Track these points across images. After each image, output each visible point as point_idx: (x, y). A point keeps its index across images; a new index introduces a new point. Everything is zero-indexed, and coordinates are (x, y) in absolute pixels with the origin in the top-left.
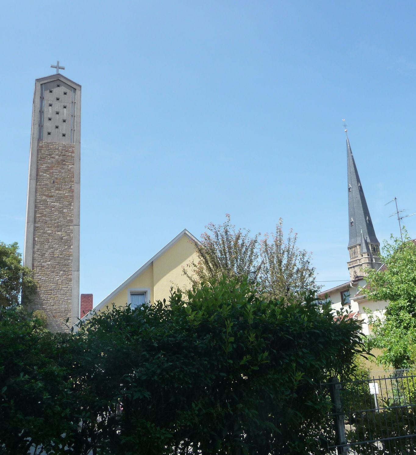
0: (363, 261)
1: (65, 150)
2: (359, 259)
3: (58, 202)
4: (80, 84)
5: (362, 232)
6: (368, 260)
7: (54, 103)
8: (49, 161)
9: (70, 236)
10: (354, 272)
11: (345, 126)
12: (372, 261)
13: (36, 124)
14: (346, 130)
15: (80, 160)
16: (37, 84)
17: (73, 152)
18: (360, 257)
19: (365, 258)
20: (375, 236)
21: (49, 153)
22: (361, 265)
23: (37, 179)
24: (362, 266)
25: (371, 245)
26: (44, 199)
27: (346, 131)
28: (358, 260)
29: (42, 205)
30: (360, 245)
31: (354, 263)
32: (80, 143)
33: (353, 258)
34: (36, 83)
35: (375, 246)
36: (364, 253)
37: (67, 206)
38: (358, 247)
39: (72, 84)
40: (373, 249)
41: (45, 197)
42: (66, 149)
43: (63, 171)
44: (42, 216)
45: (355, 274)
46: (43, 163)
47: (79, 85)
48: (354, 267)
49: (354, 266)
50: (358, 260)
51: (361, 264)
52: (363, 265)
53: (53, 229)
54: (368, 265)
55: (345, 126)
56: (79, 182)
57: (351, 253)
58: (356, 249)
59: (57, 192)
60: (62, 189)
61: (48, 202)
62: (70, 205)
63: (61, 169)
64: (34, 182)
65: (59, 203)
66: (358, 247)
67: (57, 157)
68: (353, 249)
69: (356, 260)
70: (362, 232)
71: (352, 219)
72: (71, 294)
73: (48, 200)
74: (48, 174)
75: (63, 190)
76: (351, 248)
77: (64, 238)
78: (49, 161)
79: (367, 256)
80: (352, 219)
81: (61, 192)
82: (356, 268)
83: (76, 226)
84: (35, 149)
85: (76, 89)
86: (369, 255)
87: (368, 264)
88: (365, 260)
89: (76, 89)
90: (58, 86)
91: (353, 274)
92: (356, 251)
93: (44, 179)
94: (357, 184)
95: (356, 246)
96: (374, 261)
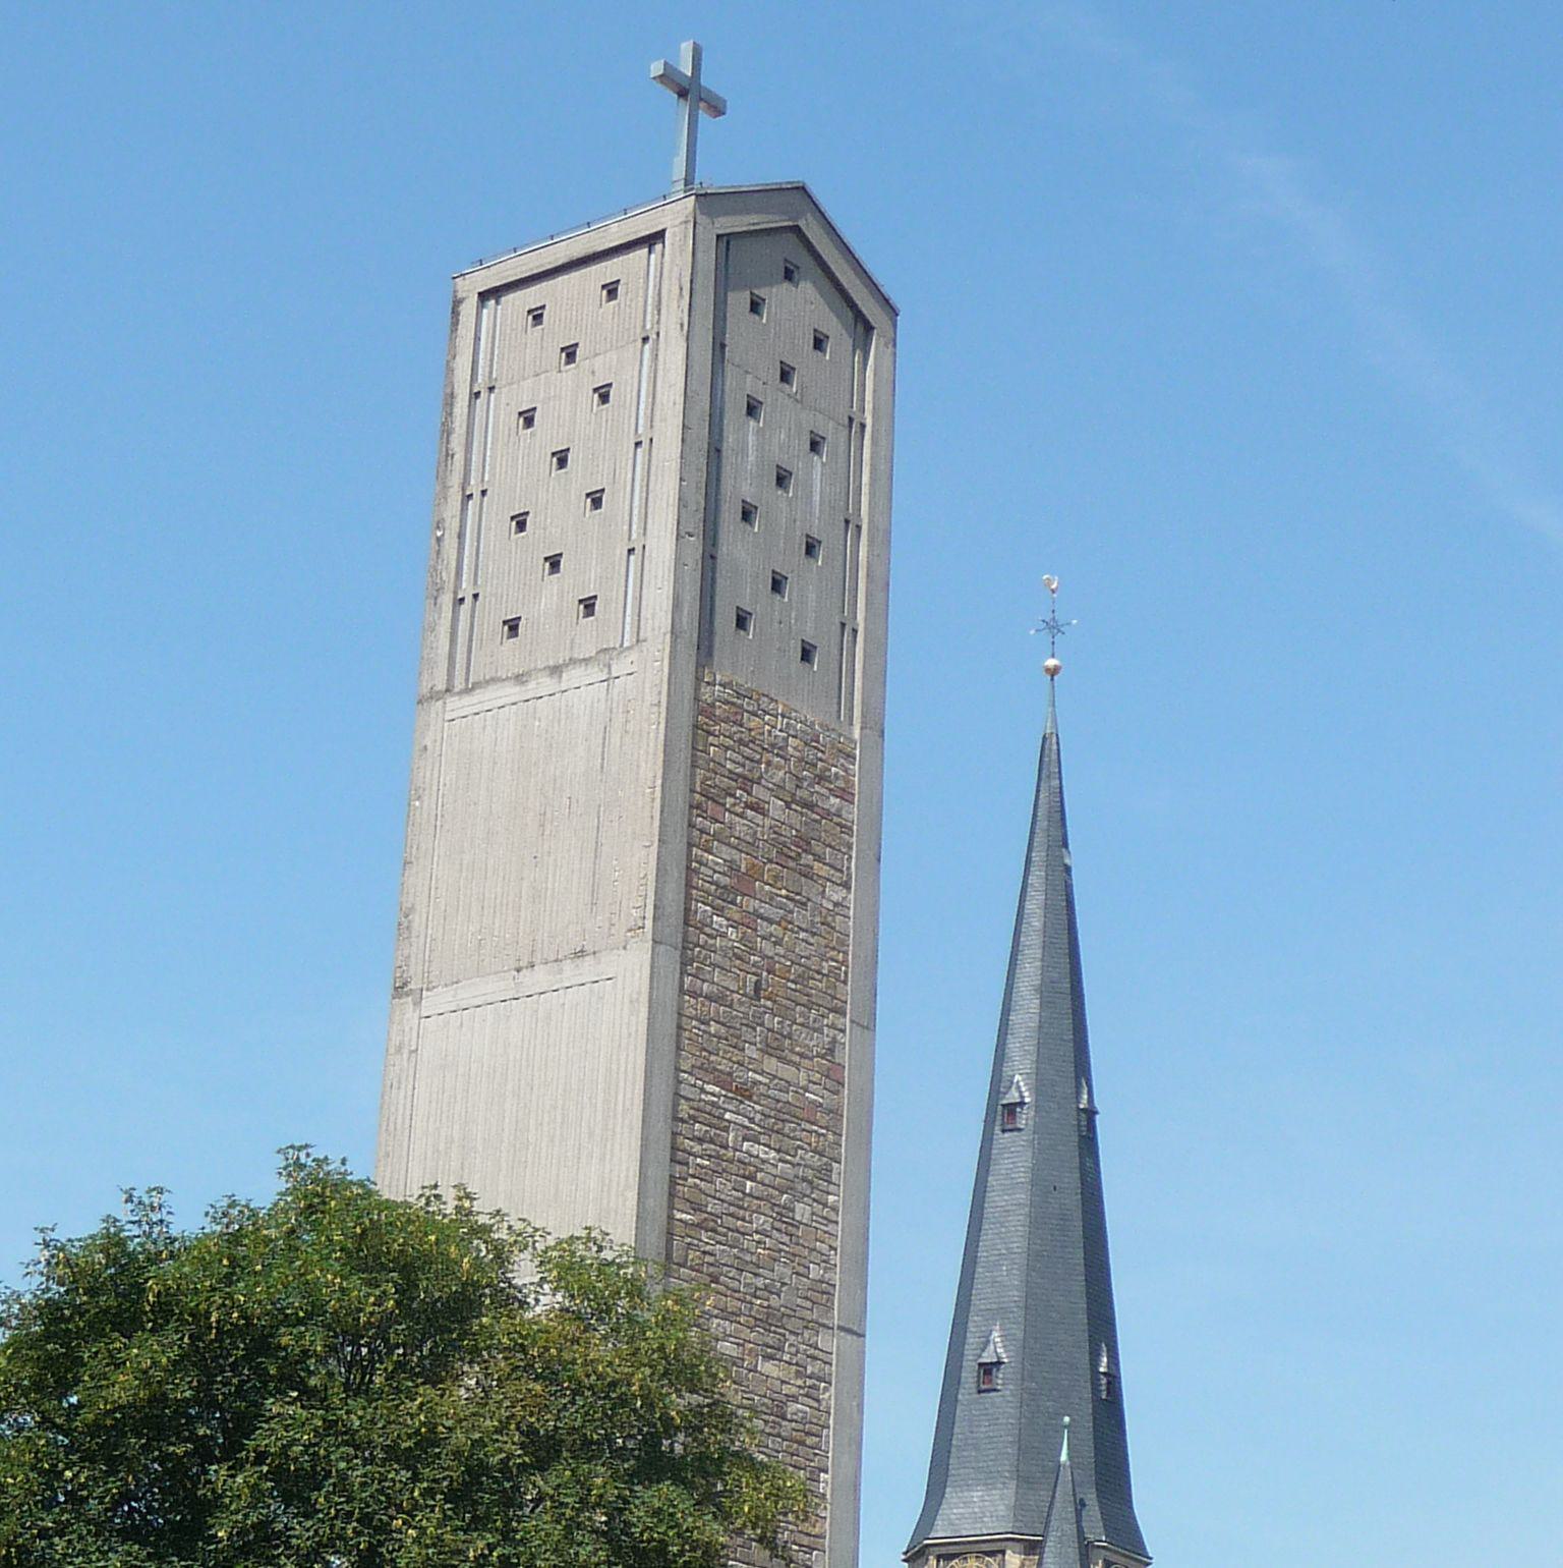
1: (815, 765)
3: (774, 1140)
4: (896, 299)
5: (1064, 1457)
8: (741, 827)
9: (818, 1401)
11: (1053, 627)
14: (1051, 662)
15: (879, 860)
16: (700, 229)
17: (845, 794)
20: (1131, 1507)
21: (739, 770)
23: (686, 945)
26: (713, 1104)
27: (1053, 672)
29: (700, 1140)
32: (882, 734)
37: (810, 1183)
39: (851, 274)
41: (718, 1089)
42: (820, 764)
43: (799, 917)
46: (716, 837)
47: (887, 301)
53: (746, 1333)
55: (1053, 627)
56: (867, 1024)
59: (770, 1065)
60: (792, 1051)
61: (726, 1130)
62: (825, 1173)
63: (791, 905)
64: (671, 960)
65: (778, 1151)
67: (776, 806)
70: (1064, 1457)
71: (996, 1336)
73: (727, 1116)
74: (734, 925)
75: (797, 1059)
76: (950, 1557)
77: (793, 1407)
80: (996, 1336)
81: (787, 1072)
83: (849, 1337)
84: (685, 719)
85: (872, 328)
89: (872, 328)
90: (789, 275)
94: (1071, 1090)
95: (1003, 1552)
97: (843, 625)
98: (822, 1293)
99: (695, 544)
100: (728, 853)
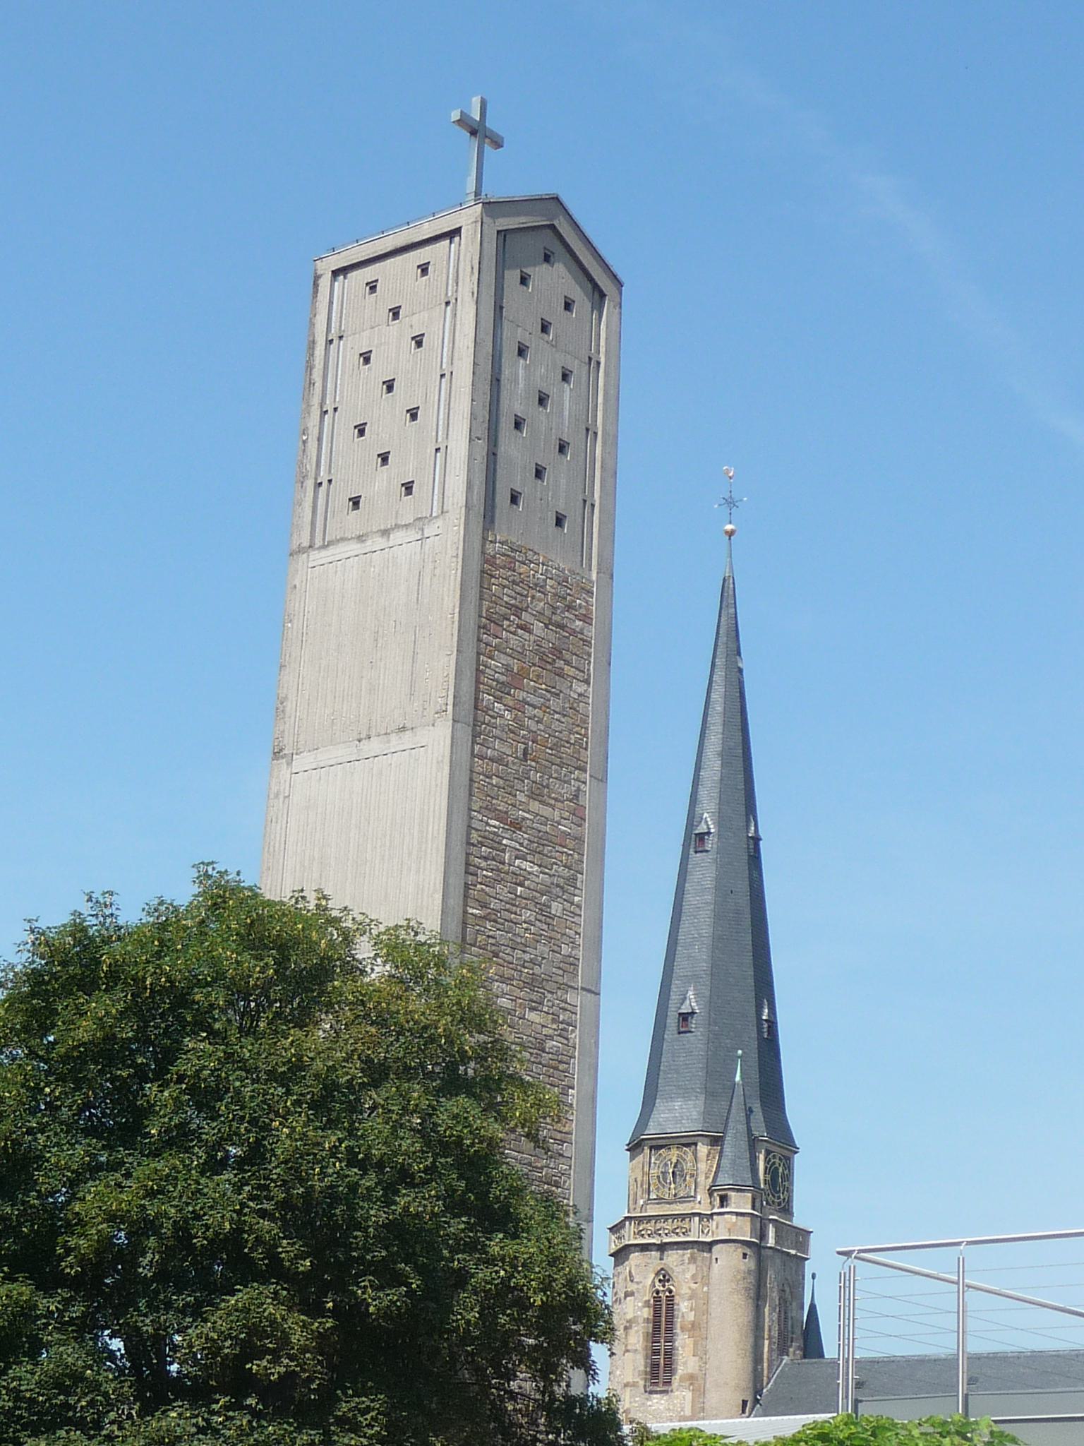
0: (720, 1229)
1: (565, 599)
2: (699, 1214)
3: (537, 858)
5: (738, 1078)
6: (748, 1228)
7: (533, 345)
8: (514, 641)
9: (567, 1039)
10: (657, 1274)
11: (730, 503)
12: (763, 1236)
13: (479, 435)
14: (729, 527)
15: (610, 664)
17: (586, 619)
18: (702, 1204)
19: (737, 1214)
22: (709, 1246)
23: (476, 723)
24: (710, 1251)
25: (768, 1152)
26: (495, 833)
27: (730, 534)
28: (697, 1219)
29: (486, 859)
30: (716, 1141)
31: (669, 1225)
32: (612, 576)
33: (660, 1200)
34: (485, 218)
35: (777, 1161)
36: (738, 1190)
37: (562, 888)
38: (703, 1149)
40: (768, 1178)
42: (569, 598)
43: (554, 703)
44: (485, 918)
45: (659, 1286)
46: (496, 648)
47: (615, 276)
48: (662, 1248)
49: (666, 1244)
50: (697, 1219)
51: (708, 1239)
52: (716, 1248)
53: (517, 992)
54: (745, 1256)
55: (730, 503)
56: (601, 778)
57: (654, 1171)
58: (690, 1156)
59: (534, 806)
61: (504, 851)
63: (548, 695)
64: (465, 733)
65: (540, 866)
66: (703, 1149)
67: (538, 627)
68: (674, 1154)
69: (683, 1217)
70: (738, 1078)
71: (691, 994)
72: (653, 1342)
75: (552, 802)
77: (550, 1044)
78: (514, 641)
79: (750, 1206)
80: (691, 994)
81: (546, 811)
82: (672, 1258)
84: (475, 567)
86: (758, 1204)
87: (748, 1251)
88: (735, 1224)
90: (547, 259)
91: (650, 1282)
92: (688, 1166)
93: (496, 732)
95: (696, 1144)
96: (771, 1242)
97: (585, 501)
98: (570, 964)
99: (482, 445)
100: (505, 659)
